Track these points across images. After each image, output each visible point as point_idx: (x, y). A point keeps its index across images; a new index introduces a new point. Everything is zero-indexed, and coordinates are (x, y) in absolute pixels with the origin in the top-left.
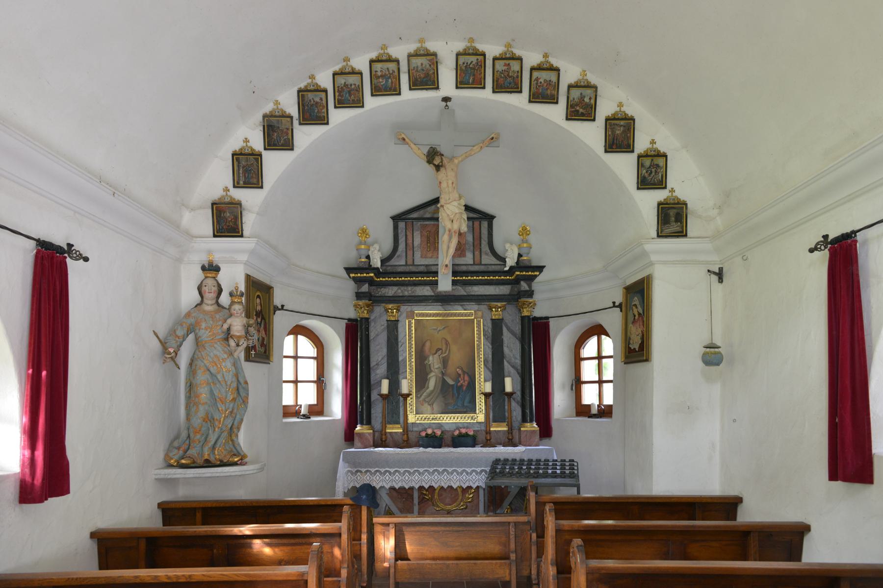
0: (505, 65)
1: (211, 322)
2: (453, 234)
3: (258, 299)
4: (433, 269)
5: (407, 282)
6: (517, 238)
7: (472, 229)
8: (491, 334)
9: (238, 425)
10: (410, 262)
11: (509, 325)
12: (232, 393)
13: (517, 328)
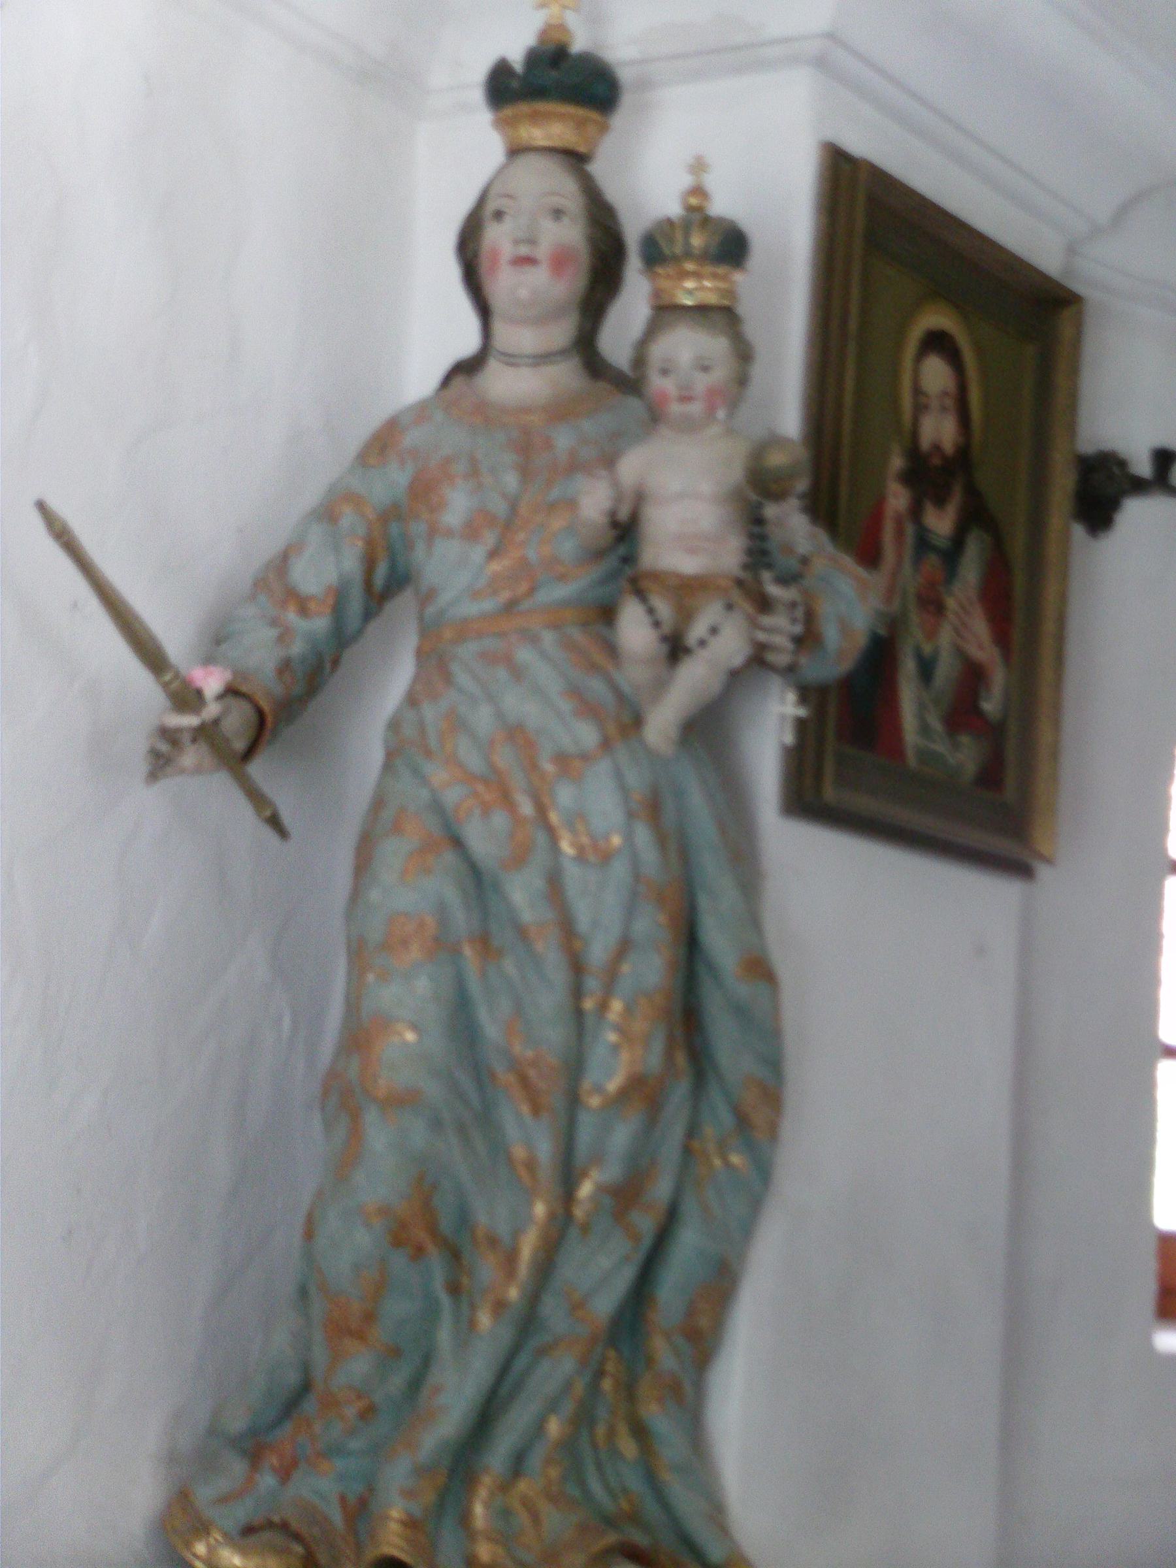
1: (511, 480)
9: (691, 1312)
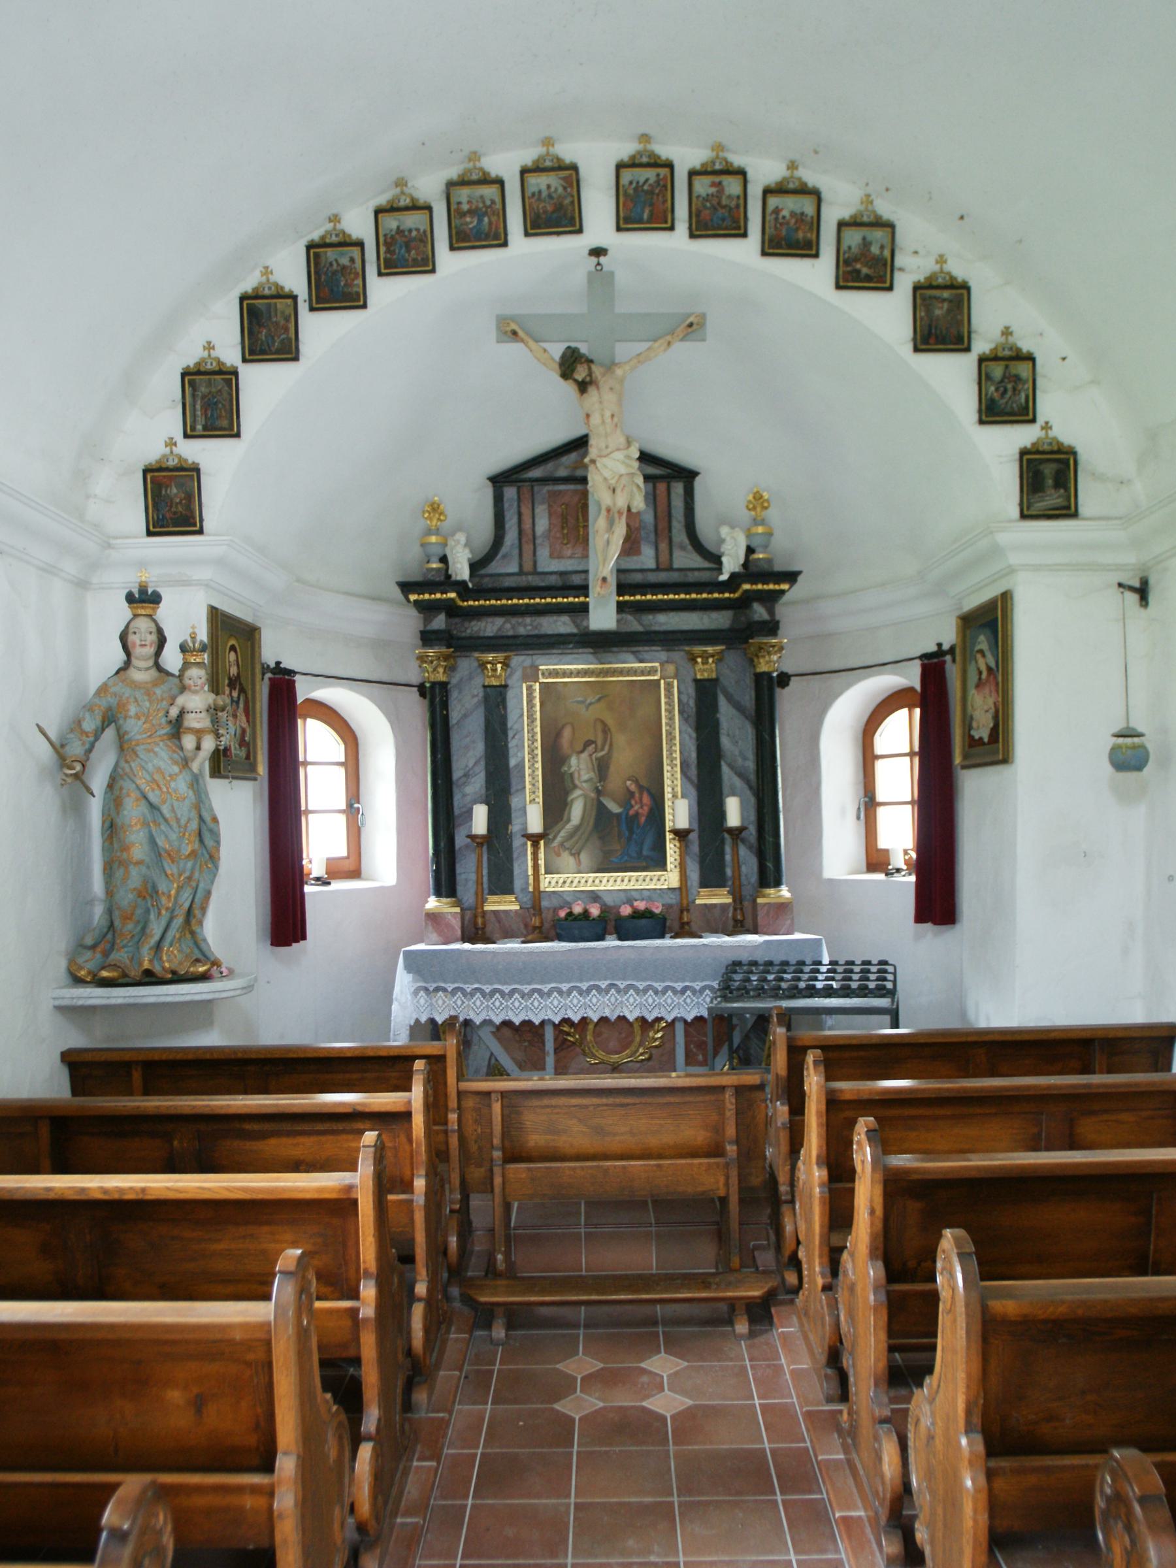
0: (713, 184)
1: (147, 704)
2: (616, 515)
3: (232, 654)
4: (576, 580)
5: (523, 608)
6: (745, 516)
7: (652, 499)
8: (694, 710)
10: (528, 567)
11: (730, 690)
12: (190, 842)
13: (747, 697)
